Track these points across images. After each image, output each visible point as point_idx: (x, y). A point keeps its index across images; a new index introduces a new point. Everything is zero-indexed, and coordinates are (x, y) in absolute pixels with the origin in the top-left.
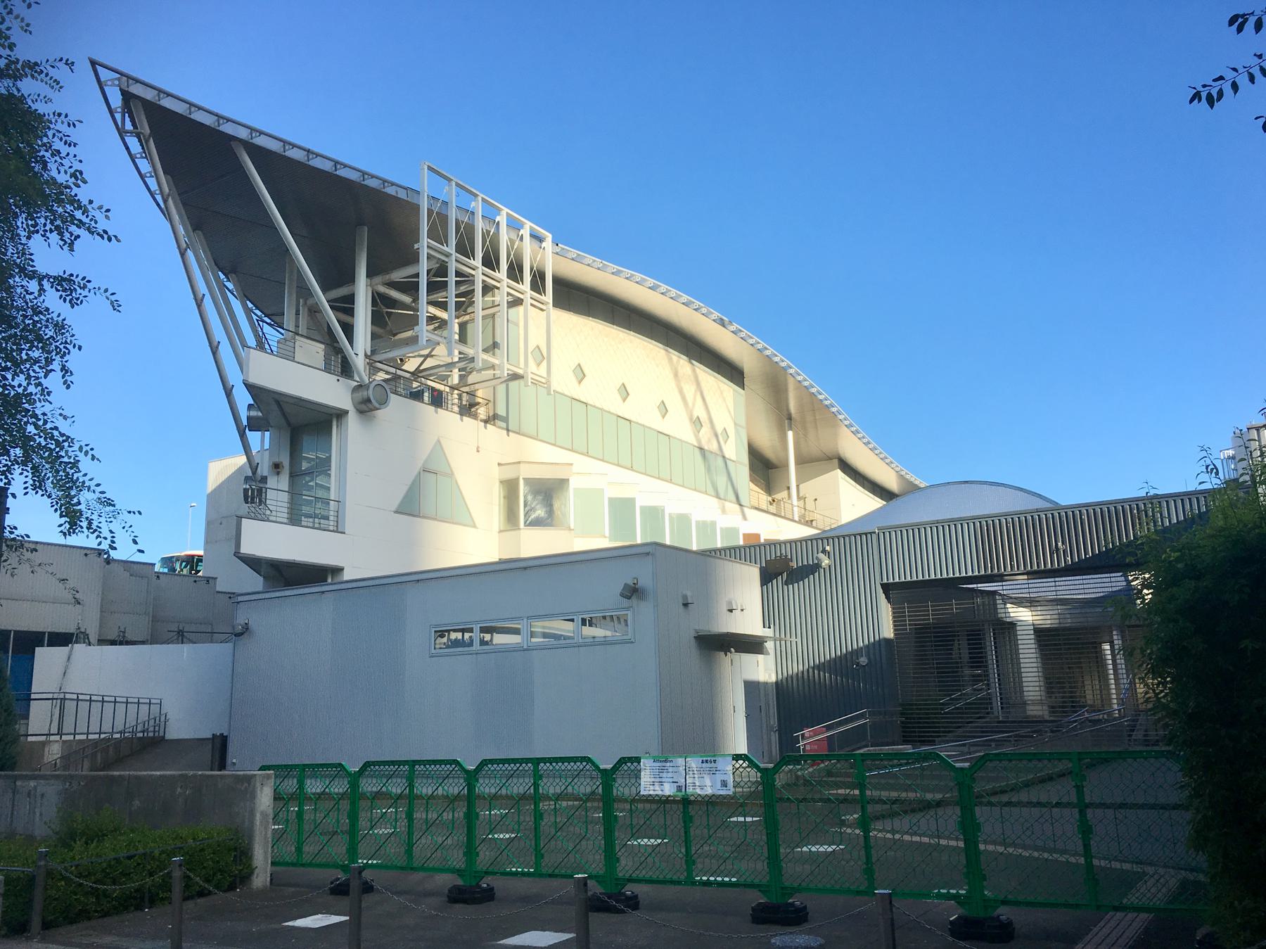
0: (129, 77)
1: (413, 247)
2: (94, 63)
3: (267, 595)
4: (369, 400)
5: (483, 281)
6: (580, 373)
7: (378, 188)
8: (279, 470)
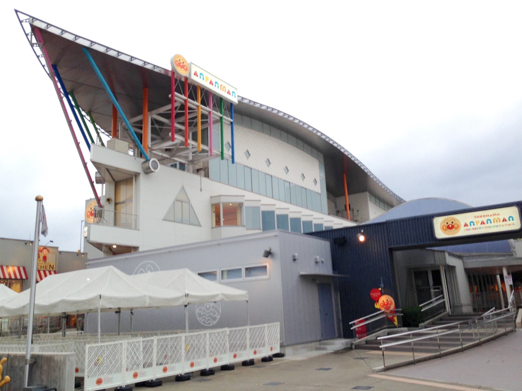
0: (33, 18)
2: (16, 11)
4: (149, 168)
5: (201, 112)
6: (248, 154)
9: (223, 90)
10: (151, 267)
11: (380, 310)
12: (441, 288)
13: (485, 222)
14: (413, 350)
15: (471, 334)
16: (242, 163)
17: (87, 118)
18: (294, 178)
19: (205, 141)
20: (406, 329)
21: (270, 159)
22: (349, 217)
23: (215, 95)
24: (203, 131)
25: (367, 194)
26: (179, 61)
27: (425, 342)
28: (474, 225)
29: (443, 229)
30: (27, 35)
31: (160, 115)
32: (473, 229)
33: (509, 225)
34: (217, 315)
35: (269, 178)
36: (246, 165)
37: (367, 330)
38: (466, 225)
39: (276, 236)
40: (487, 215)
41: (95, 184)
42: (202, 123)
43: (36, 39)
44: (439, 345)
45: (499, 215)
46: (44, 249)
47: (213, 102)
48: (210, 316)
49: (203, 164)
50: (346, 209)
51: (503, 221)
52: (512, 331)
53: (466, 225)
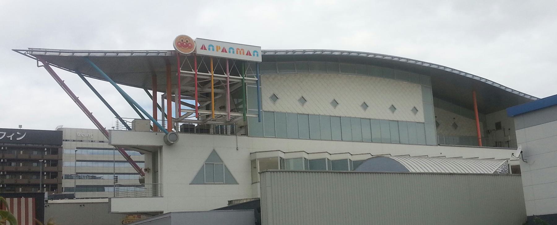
10: (2, 197)
21: (394, 105)
26: (186, 42)
51: (247, 54)
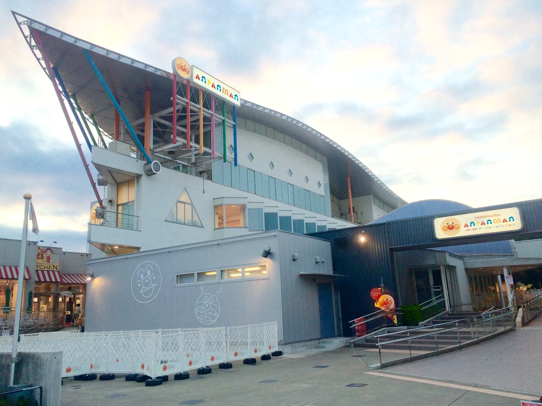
1: (170, 99)
2: (14, 13)
3: (111, 259)
5: (203, 114)
6: (251, 156)
7: (116, 59)
8: (112, 203)
9: (225, 94)
11: (379, 309)
12: (441, 288)
13: (486, 223)
14: (410, 348)
15: (469, 333)
16: (245, 166)
17: (90, 122)
18: (298, 181)
19: (208, 143)
20: (405, 327)
22: (353, 219)
23: (217, 98)
24: (205, 134)
25: (371, 197)
27: (398, 345)
28: (474, 225)
29: (444, 230)
30: (26, 37)
31: (162, 117)
32: (474, 229)
33: (510, 225)
34: (216, 315)
35: (272, 182)
36: (249, 168)
37: (369, 327)
38: (466, 226)
39: (275, 235)
40: (488, 215)
41: (97, 185)
42: (205, 126)
43: (35, 41)
44: (437, 343)
45: (500, 215)
46: (47, 249)
47: (190, 94)
48: (209, 315)
49: (206, 166)
50: (350, 213)
51: (504, 221)
52: (511, 330)
53: (466, 226)
